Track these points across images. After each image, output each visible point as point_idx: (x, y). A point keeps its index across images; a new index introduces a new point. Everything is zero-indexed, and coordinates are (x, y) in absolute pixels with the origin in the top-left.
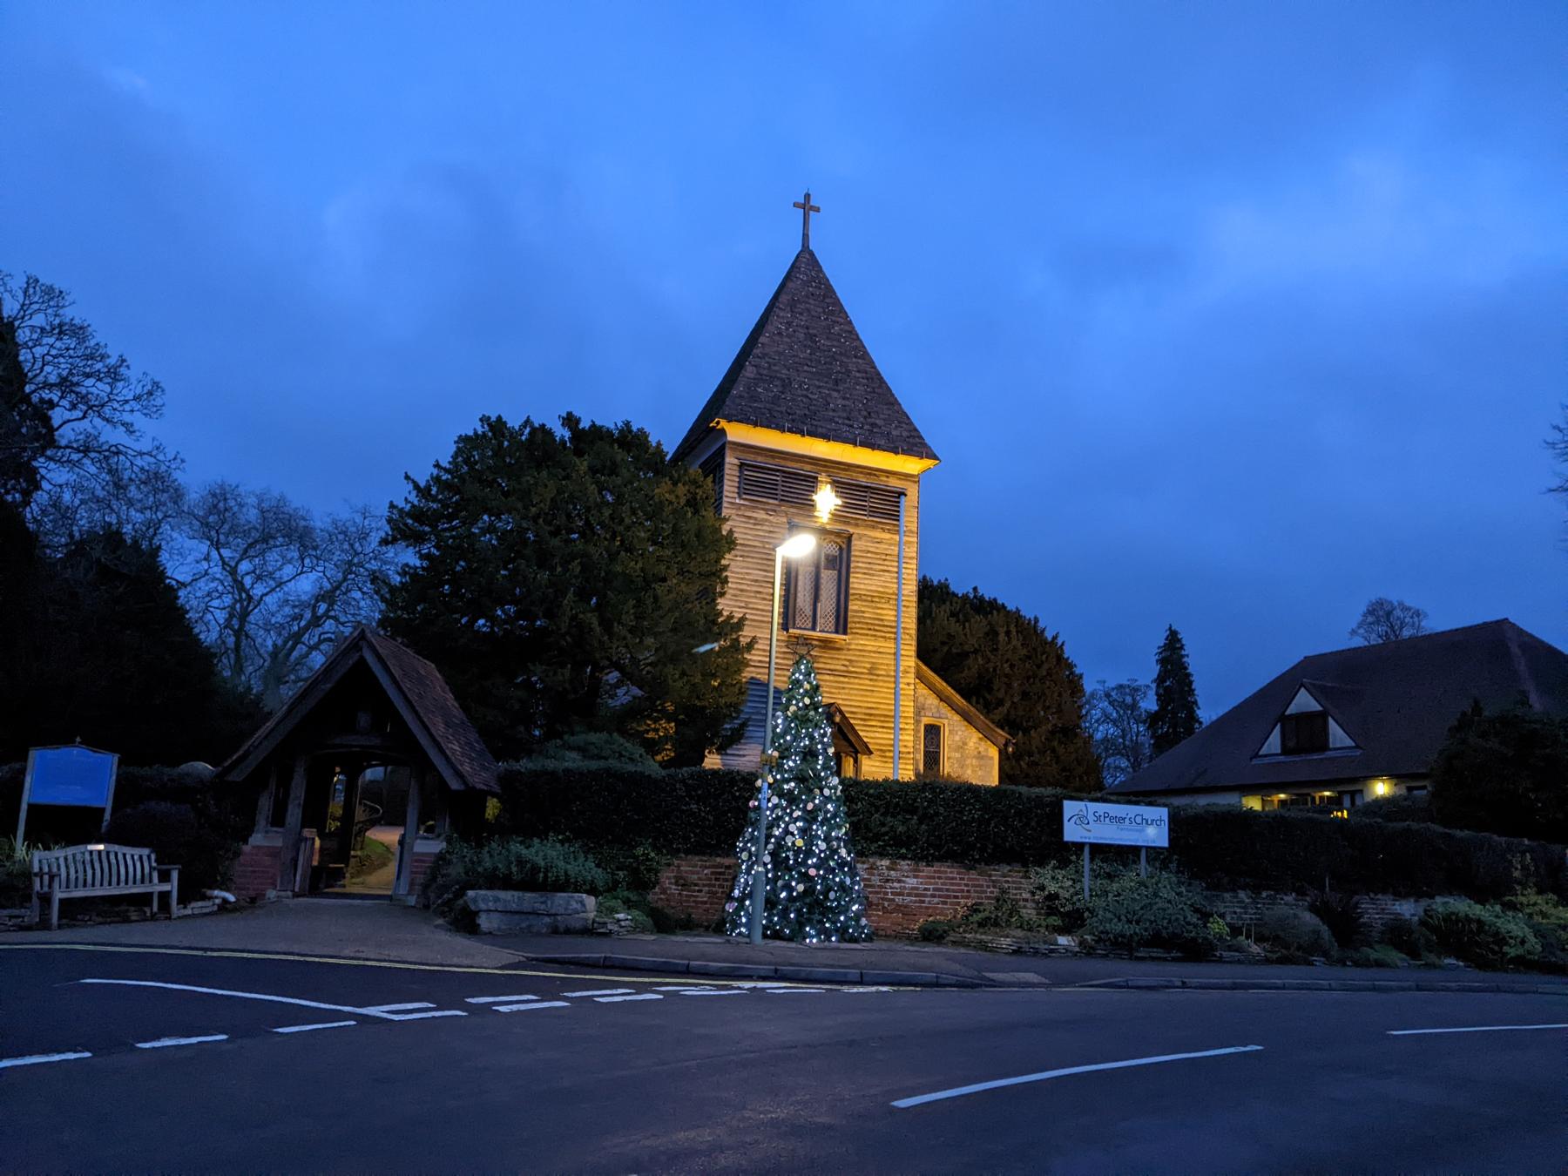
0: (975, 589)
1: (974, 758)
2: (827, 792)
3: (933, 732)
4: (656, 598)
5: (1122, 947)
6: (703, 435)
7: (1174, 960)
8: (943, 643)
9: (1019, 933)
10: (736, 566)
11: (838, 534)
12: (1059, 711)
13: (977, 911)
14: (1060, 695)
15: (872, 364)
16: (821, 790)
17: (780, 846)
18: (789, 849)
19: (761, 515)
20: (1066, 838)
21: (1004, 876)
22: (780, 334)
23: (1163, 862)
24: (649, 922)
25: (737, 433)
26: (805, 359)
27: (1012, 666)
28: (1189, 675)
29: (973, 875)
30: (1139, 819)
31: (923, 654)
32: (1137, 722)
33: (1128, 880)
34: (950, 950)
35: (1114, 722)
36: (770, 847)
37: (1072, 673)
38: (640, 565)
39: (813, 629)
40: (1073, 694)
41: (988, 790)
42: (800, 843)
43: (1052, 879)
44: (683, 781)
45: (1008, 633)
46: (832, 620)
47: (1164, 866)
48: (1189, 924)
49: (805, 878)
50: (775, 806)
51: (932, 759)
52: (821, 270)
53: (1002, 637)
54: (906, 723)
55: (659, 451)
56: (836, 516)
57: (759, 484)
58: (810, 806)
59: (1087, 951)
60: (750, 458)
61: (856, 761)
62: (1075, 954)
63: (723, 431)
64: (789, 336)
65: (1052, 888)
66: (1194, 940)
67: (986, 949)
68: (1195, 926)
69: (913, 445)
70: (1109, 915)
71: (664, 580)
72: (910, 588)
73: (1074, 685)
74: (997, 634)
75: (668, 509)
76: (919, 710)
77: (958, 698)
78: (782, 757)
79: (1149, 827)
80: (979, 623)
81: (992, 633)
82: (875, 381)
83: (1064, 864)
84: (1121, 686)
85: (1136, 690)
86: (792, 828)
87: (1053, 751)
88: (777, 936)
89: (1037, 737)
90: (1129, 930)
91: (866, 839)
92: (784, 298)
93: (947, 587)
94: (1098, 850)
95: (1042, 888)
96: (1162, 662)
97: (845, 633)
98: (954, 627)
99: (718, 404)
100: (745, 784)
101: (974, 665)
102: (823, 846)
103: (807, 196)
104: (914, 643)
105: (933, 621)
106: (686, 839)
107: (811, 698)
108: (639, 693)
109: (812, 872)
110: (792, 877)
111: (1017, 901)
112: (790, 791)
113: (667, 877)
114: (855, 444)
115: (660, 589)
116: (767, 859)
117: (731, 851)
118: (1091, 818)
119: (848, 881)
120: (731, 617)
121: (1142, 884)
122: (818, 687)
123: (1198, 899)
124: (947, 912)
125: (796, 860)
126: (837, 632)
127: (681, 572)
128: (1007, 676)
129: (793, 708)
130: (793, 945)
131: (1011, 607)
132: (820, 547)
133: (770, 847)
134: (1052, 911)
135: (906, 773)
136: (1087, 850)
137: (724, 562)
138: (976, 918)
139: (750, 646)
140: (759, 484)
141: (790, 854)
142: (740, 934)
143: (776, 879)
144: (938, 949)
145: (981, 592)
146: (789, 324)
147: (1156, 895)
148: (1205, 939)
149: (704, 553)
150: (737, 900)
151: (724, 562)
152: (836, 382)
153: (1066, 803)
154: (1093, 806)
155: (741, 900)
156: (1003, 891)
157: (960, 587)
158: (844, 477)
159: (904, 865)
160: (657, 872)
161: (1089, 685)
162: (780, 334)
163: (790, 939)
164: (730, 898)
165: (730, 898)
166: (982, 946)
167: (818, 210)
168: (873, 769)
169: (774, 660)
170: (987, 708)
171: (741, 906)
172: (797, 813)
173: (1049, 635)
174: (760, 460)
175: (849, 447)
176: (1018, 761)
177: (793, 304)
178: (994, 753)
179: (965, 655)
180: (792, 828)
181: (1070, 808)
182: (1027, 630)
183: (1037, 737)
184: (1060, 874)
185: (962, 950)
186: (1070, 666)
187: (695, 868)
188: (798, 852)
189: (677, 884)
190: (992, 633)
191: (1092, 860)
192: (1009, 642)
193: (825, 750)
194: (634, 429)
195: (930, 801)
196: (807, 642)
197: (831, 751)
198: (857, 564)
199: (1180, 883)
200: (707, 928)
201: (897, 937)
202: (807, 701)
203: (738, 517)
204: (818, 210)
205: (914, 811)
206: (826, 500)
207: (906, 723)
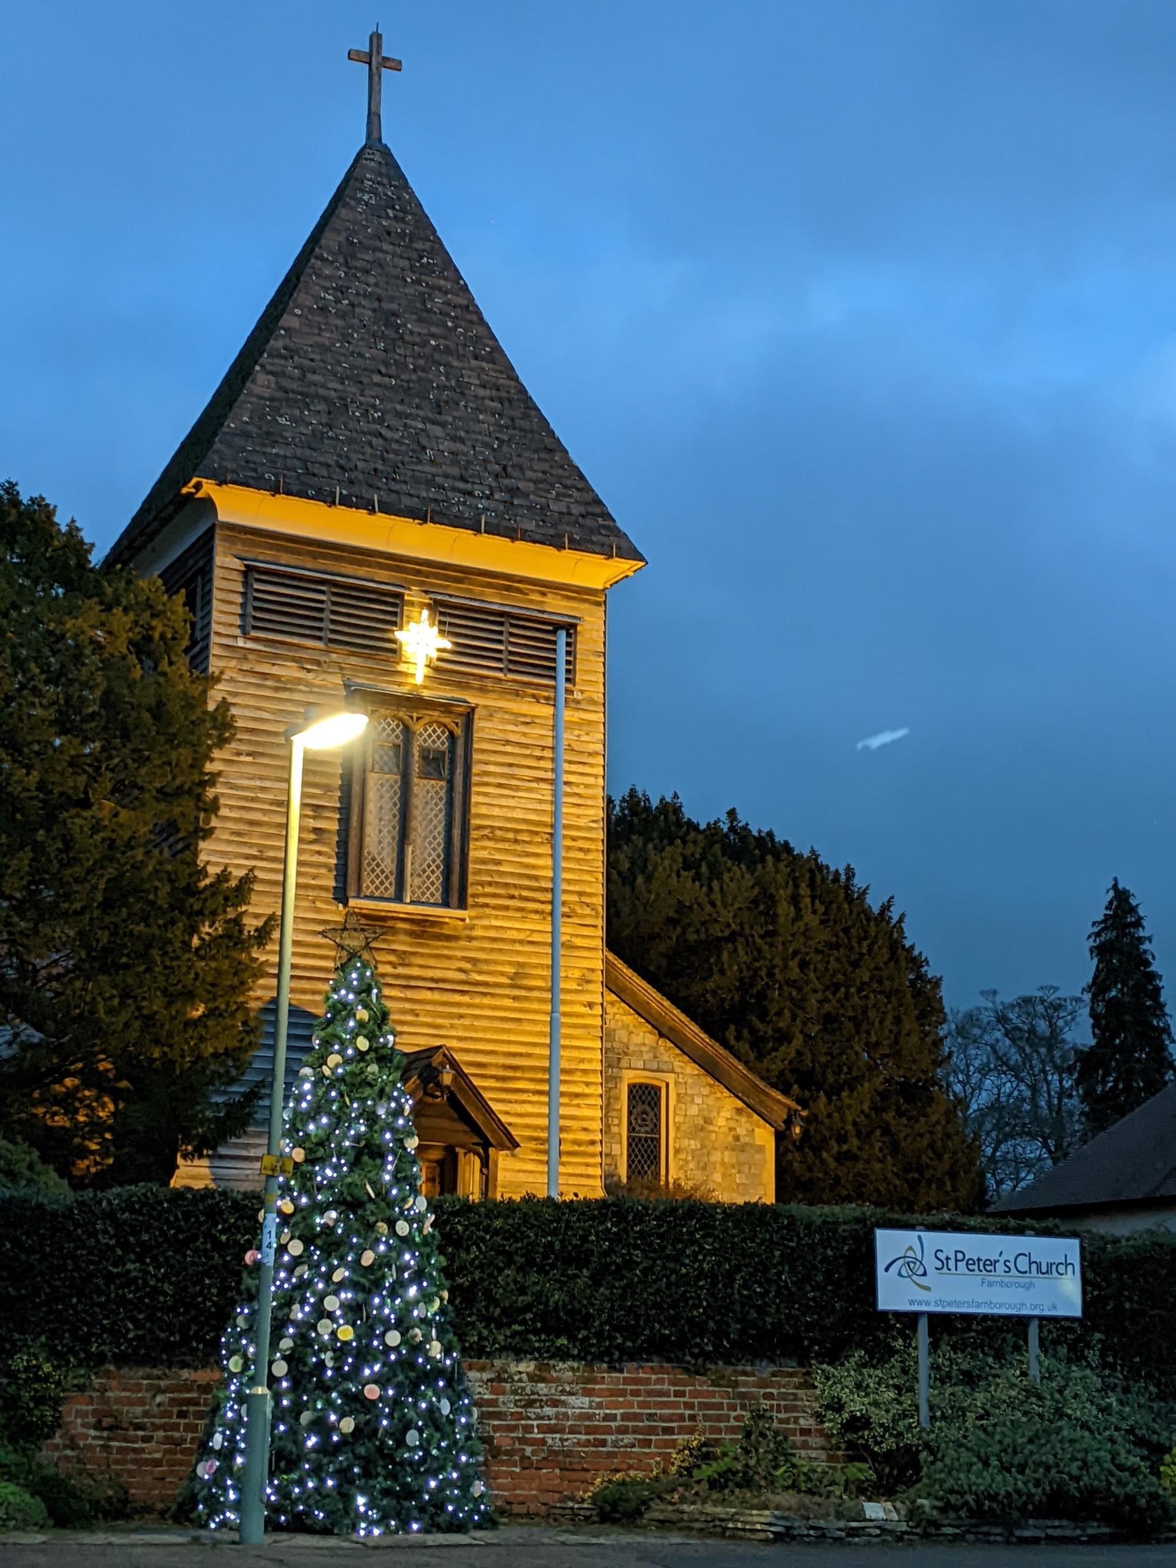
0: (732, 814)
1: (725, 1148)
2: (402, 1228)
3: (646, 1099)
4: (68, 842)
5: (988, 1519)
6: (171, 510)
7: (1094, 1540)
8: (670, 921)
9: (789, 1499)
10: (230, 771)
11: (446, 707)
12: (896, 1054)
13: (707, 1457)
14: (898, 1021)
15: (510, 372)
16: (391, 1223)
17: (304, 1340)
18: (323, 1349)
19: (288, 671)
20: (882, 1305)
21: (763, 1384)
22: (323, 310)
23: (1072, 1348)
24: (37, 1507)
25: (237, 505)
26: (377, 366)
27: (804, 965)
28: (1153, 976)
29: (702, 1385)
30: (1023, 1263)
31: (616, 941)
32: (1058, 1069)
33: (1005, 1385)
34: (651, 1540)
35: (1016, 1071)
36: (286, 1344)
37: (920, 977)
38: (35, 775)
39: (399, 898)
40: (923, 1016)
41: (750, 1214)
42: (346, 1333)
43: (855, 1388)
44: (111, 1215)
45: (795, 900)
46: (437, 878)
47: (1076, 1356)
48: (1121, 1468)
49: (356, 1403)
50: (297, 1261)
51: (645, 1150)
52: (405, 186)
53: (784, 909)
54: (582, 1078)
55: (76, 546)
56: (440, 671)
57: (286, 608)
58: (368, 1258)
59: (924, 1530)
60: (264, 557)
61: (485, 1163)
62: (900, 1538)
63: (209, 503)
64: (342, 315)
65: (856, 1405)
66: (1130, 1499)
67: (723, 1533)
68: (1134, 1471)
69: (593, 529)
70: (965, 1456)
71: (86, 804)
72: (587, 818)
73: (925, 999)
74: (772, 900)
75: (92, 660)
76: (613, 1059)
77: (693, 1031)
78: (311, 1161)
79: (1041, 1278)
80: (739, 881)
81: (764, 902)
82: (517, 404)
83: (879, 1354)
84: (1027, 1000)
85: (1057, 1007)
86: (331, 1303)
87: (886, 1130)
88: (299, 1525)
89: (856, 1104)
90: (1004, 1484)
91: (487, 1320)
92: (331, 240)
93: (677, 810)
94: (942, 1324)
95: (837, 1406)
96: (1102, 951)
97: (462, 905)
98: (690, 890)
99: (197, 451)
100: (238, 1215)
101: (733, 962)
102: (393, 1338)
103: (376, 39)
104: (601, 922)
105: (649, 879)
106: (116, 1333)
107: (371, 1037)
108: (37, 1037)
109: (372, 1392)
110: (329, 1403)
111: (786, 1434)
112: (328, 1230)
113: (78, 1414)
114: (477, 530)
115: (77, 822)
116: (280, 1369)
117: (211, 1355)
118: (931, 1263)
119: (445, 1407)
120: (224, 877)
121: (1029, 1392)
122: (385, 1016)
123: (1136, 1417)
124: (652, 1462)
125: (337, 1369)
126: (446, 904)
127: (120, 790)
128: (793, 984)
129: (334, 1059)
130: (332, 1542)
131: (801, 848)
132: (364, 739)
133: (286, 1344)
134: (856, 1452)
135: (582, 1181)
136: (923, 1325)
137: (209, 767)
138: (708, 1470)
139: (262, 935)
140: (286, 608)
141: (327, 1357)
142: (223, 1524)
143: (297, 1409)
144: (626, 1539)
145: (743, 818)
146: (342, 290)
147: (1059, 1413)
148: (1154, 1496)
149: (164, 743)
150: (219, 1454)
151: (209, 767)
152: (438, 408)
153: (881, 1235)
154: (934, 1239)
155: (226, 1456)
156: (758, 1416)
157: (702, 811)
158: (457, 594)
159: (564, 1370)
160: (57, 1402)
161: (956, 999)
162: (323, 310)
163: (326, 1531)
164: (204, 1450)
165: (204, 1450)
166: (718, 1529)
167: (397, 66)
168: (517, 1176)
169: (289, 959)
170: (757, 1050)
171: (227, 1469)
172: (340, 1274)
173: (874, 902)
174: (287, 562)
175: (465, 535)
176: (817, 1150)
177: (349, 252)
178: (765, 1137)
179: (716, 944)
180: (331, 1297)
181: (890, 1244)
182: (829, 890)
183: (856, 1104)
184: (871, 1376)
185: (676, 1539)
186: (917, 963)
187: (134, 1392)
188: (341, 1351)
189: (98, 1426)
190: (764, 902)
191: (934, 1346)
192: (798, 917)
193: (400, 1142)
194: (25, 498)
195: (616, 1239)
196: (378, 924)
197: (412, 1144)
198: (486, 766)
199: (1106, 1388)
200: (162, 1514)
201: (550, 1517)
202: (363, 1044)
203: (234, 676)
204: (397, 66)
205: (580, 1259)
206: (421, 641)
207: (582, 1078)
